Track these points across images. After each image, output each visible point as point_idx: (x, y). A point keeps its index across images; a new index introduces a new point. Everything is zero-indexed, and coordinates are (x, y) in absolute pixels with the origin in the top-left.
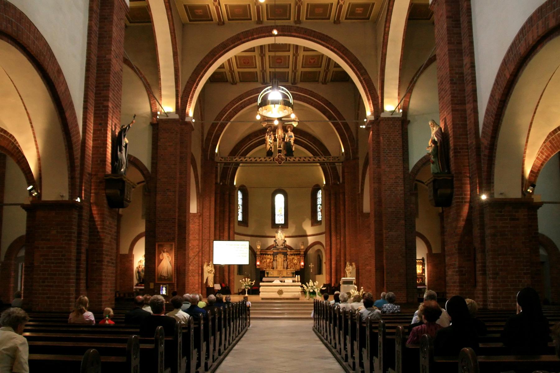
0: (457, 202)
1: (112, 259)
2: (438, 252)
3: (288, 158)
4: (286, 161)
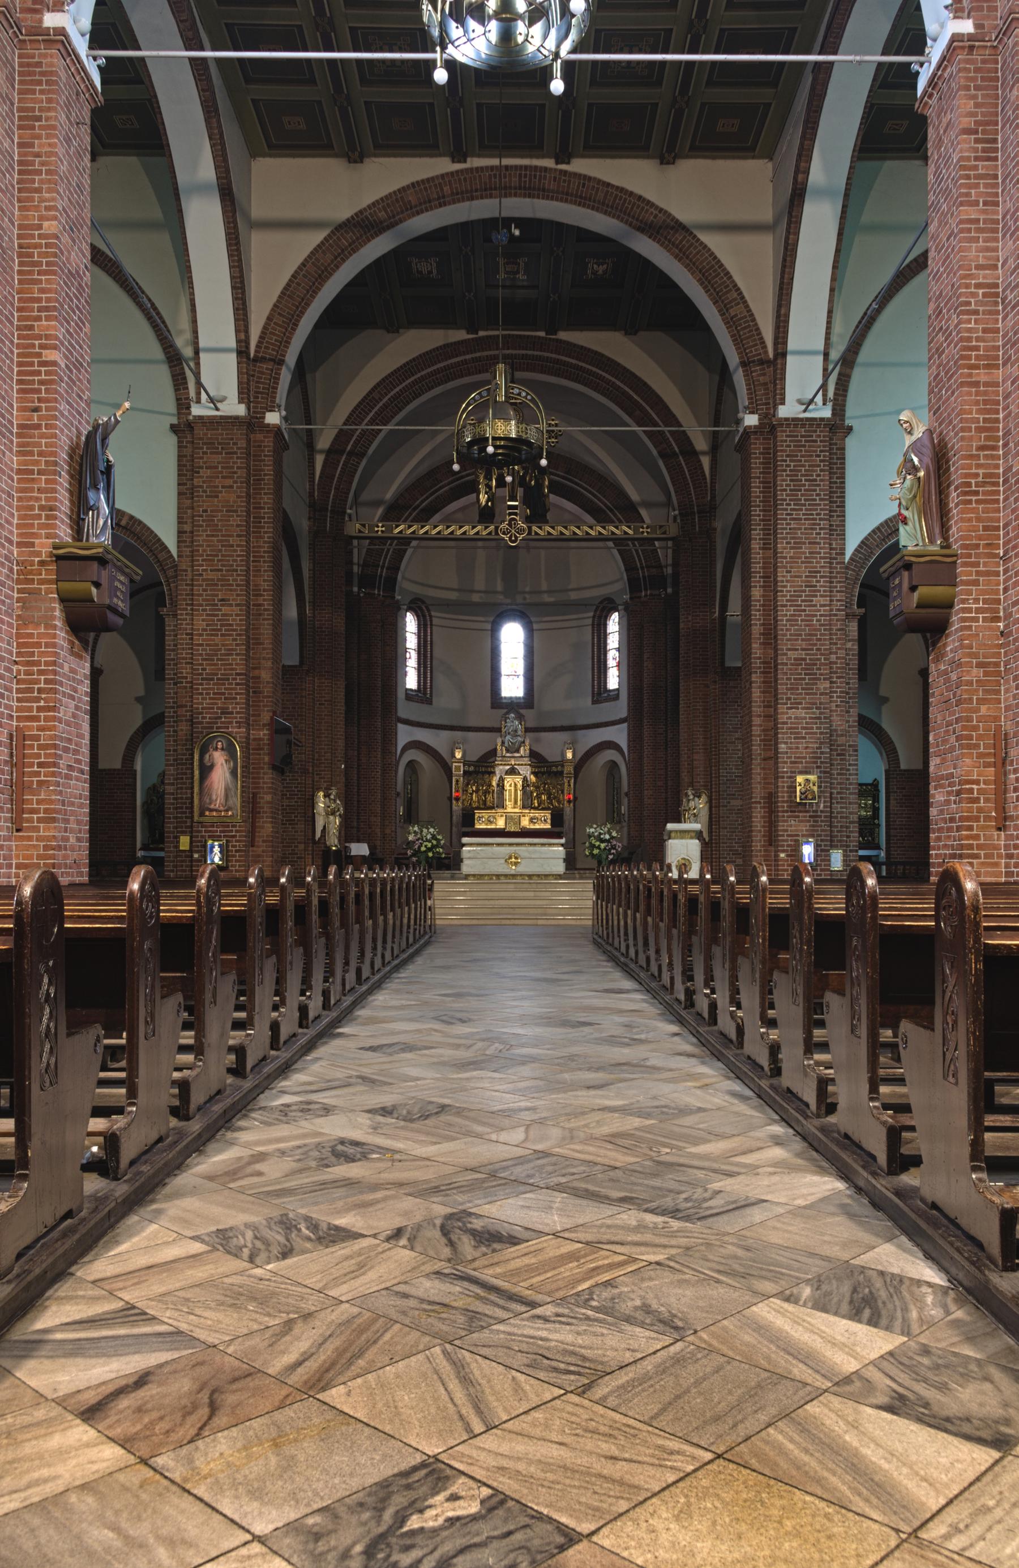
0: (964, 620)
1: (79, 762)
2: (913, 767)
3: (534, 528)
4: (529, 533)
